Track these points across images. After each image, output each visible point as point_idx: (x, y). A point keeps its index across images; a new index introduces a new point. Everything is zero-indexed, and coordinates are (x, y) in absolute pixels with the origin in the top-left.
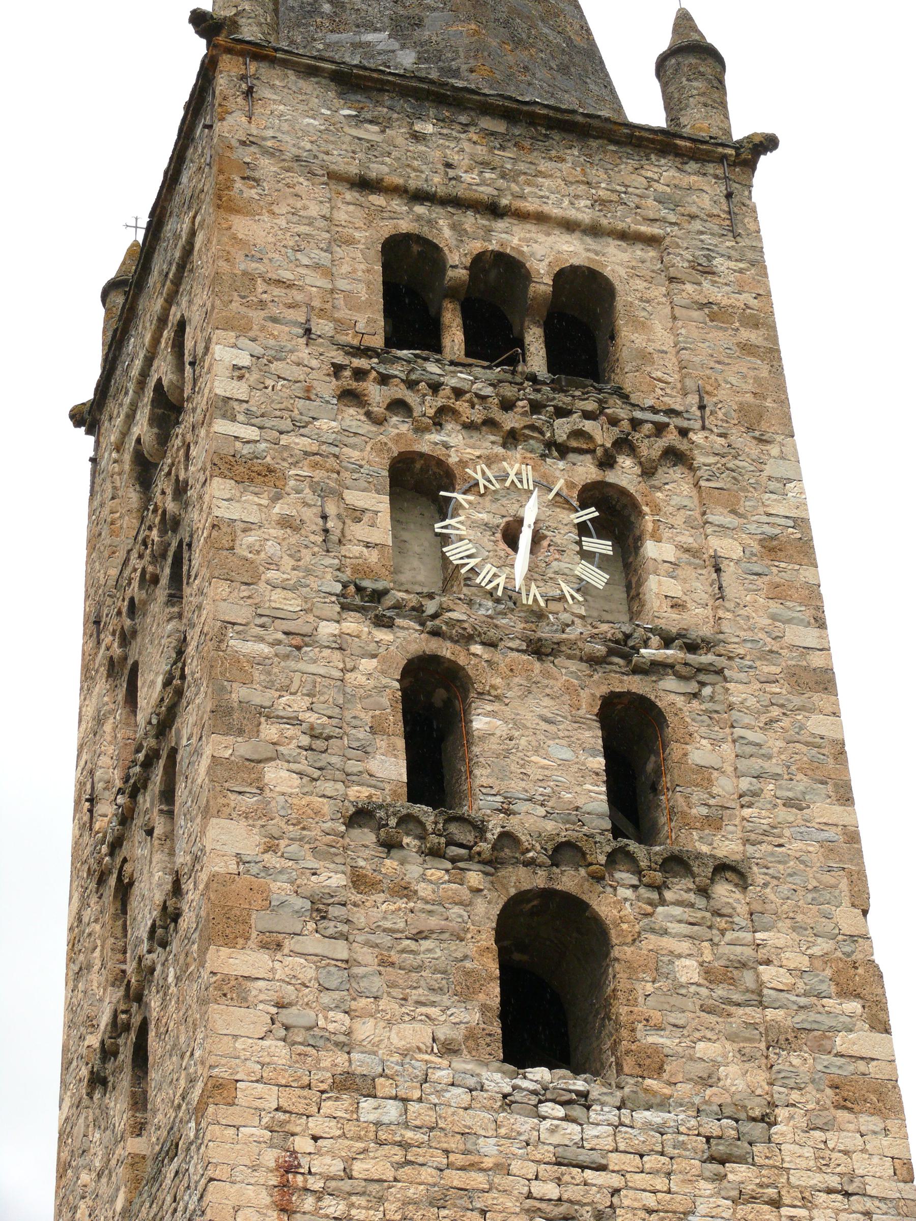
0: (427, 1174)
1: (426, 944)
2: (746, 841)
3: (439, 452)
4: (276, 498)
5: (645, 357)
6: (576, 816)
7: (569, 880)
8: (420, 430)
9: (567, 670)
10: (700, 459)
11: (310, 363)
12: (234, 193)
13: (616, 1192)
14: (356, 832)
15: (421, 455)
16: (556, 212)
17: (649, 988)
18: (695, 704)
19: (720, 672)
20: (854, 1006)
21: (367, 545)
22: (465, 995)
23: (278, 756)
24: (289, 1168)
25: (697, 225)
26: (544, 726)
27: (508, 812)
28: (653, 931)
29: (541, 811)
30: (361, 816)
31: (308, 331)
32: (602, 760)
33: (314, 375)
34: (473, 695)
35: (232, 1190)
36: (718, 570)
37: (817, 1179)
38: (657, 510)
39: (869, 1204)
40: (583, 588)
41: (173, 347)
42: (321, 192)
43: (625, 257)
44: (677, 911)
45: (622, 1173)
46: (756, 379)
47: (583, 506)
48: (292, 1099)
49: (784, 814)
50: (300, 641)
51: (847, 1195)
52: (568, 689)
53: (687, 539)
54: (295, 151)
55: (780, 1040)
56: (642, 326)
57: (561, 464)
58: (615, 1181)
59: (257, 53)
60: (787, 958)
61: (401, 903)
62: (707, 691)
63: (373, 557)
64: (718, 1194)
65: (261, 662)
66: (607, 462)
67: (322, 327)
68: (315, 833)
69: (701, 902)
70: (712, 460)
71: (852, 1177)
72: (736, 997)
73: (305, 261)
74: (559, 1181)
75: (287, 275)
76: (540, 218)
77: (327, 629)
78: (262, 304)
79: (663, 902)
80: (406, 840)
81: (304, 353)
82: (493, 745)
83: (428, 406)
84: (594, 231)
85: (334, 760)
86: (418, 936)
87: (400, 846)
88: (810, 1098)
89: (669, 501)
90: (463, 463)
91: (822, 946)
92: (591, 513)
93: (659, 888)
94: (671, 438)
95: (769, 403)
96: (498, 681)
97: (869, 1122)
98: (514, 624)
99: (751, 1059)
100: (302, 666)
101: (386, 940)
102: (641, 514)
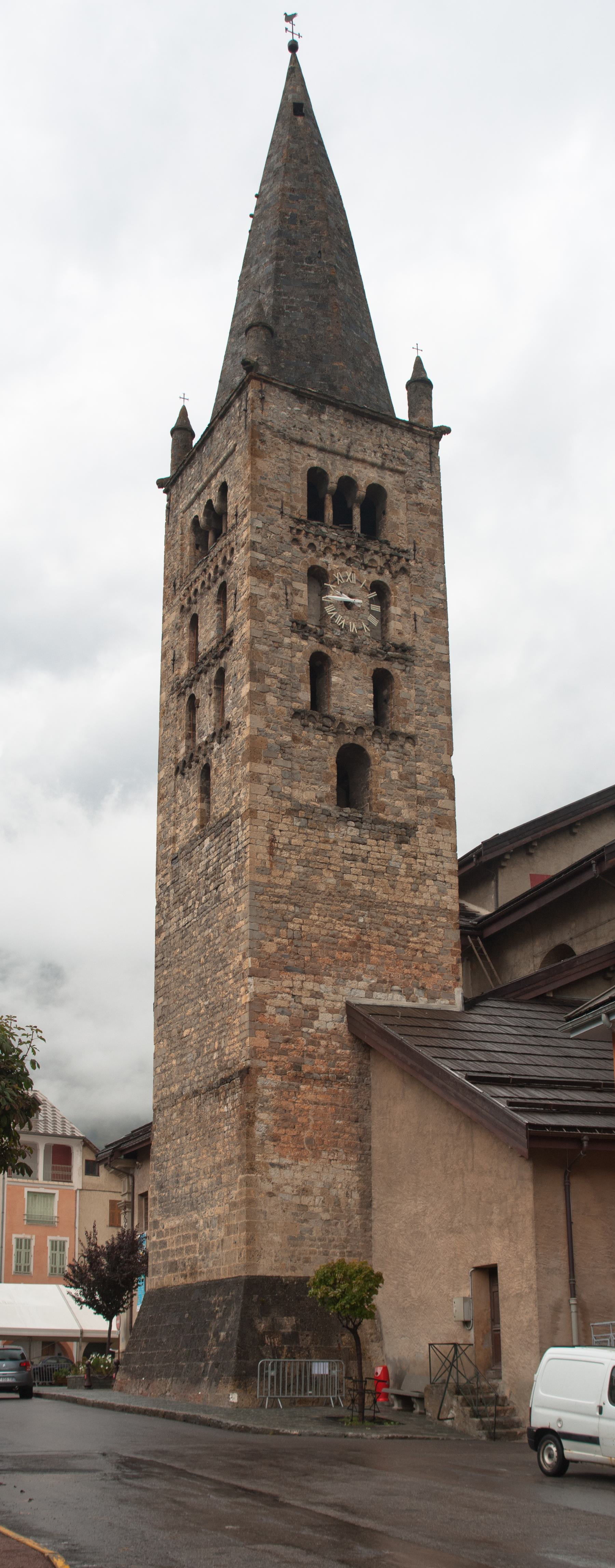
0: (313, 844)
1: (315, 763)
2: (416, 728)
3: (324, 566)
4: (271, 585)
5: (396, 526)
6: (362, 716)
7: (359, 741)
8: (318, 556)
9: (363, 659)
10: (413, 573)
11: (282, 525)
12: (257, 447)
13: (369, 852)
14: (294, 720)
15: (318, 567)
16: (369, 459)
17: (382, 781)
18: (404, 674)
19: (413, 662)
20: (444, 791)
21: (300, 605)
22: (326, 781)
23: (270, 691)
24: (273, 840)
25: (418, 467)
26: (355, 681)
27: (342, 714)
28: (385, 760)
29: (352, 714)
30: (297, 714)
31: (282, 513)
32: (372, 695)
33: (284, 531)
34: (331, 667)
35: (256, 847)
36: (415, 620)
37: (428, 850)
38: (396, 593)
39: (443, 859)
40: (369, 624)
41: (220, 490)
42: (286, 447)
43: (391, 480)
44: (393, 753)
45: (371, 846)
46: (434, 538)
47: (372, 591)
48: (273, 817)
49: (429, 718)
50: (278, 645)
51: (437, 856)
52: (363, 666)
53: (405, 606)
54: (278, 427)
55: (420, 801)
56: (396, 512)
57: (365, 573)
58: (369, 848)
59: (265, 380)
60: (425, 772)
61: (307, 747)
62: (408, 669)
63: (301, 609)
64: (399, 854)
65: (265, 653)
66: (381, 573)
67: (287, 510)
68: (282, 720)
69: (400, 750)
70: (416, 573)
71: (438, 849)
72: (409, 785)
73: (281, 480)
74: (352, 848)
75: (275, 486)
76: (363, 461)
77: (287, 640)
78: (266, 500)
79: (388, 750)
80: (310, 724)
81: (280, 522)
82: (338, 688)
83: (321, 547)
84: (382, 467)
85: (288, 693)
86: (312, 760)
87: (308, 726)
88: (428, 822)
89: (400, 587)
90: (332, 571)
91: (437, 769)
92: (374, 594)
93: (388, 745)
94: (403, 562)
95: (437, 549)
96: (341, 663)
97: (445, 831)
98: (346, 640)
99: (412, 807)
100: (278, 655)
101: (302, 761)
102: (390, 593)
